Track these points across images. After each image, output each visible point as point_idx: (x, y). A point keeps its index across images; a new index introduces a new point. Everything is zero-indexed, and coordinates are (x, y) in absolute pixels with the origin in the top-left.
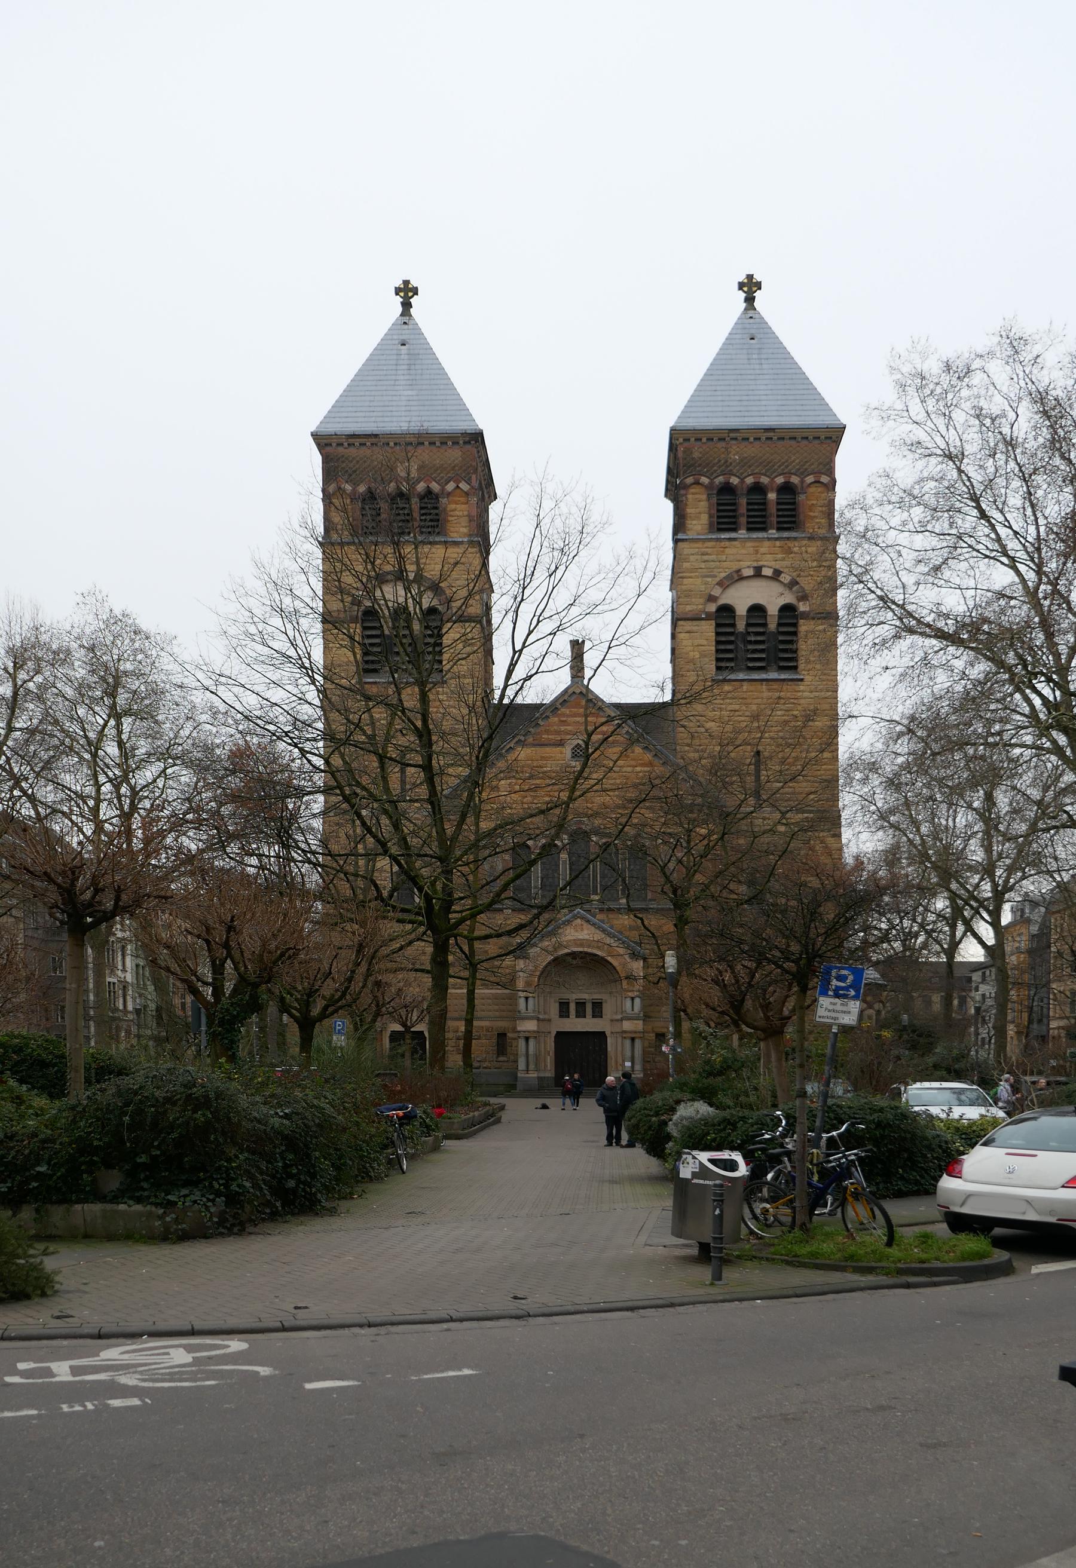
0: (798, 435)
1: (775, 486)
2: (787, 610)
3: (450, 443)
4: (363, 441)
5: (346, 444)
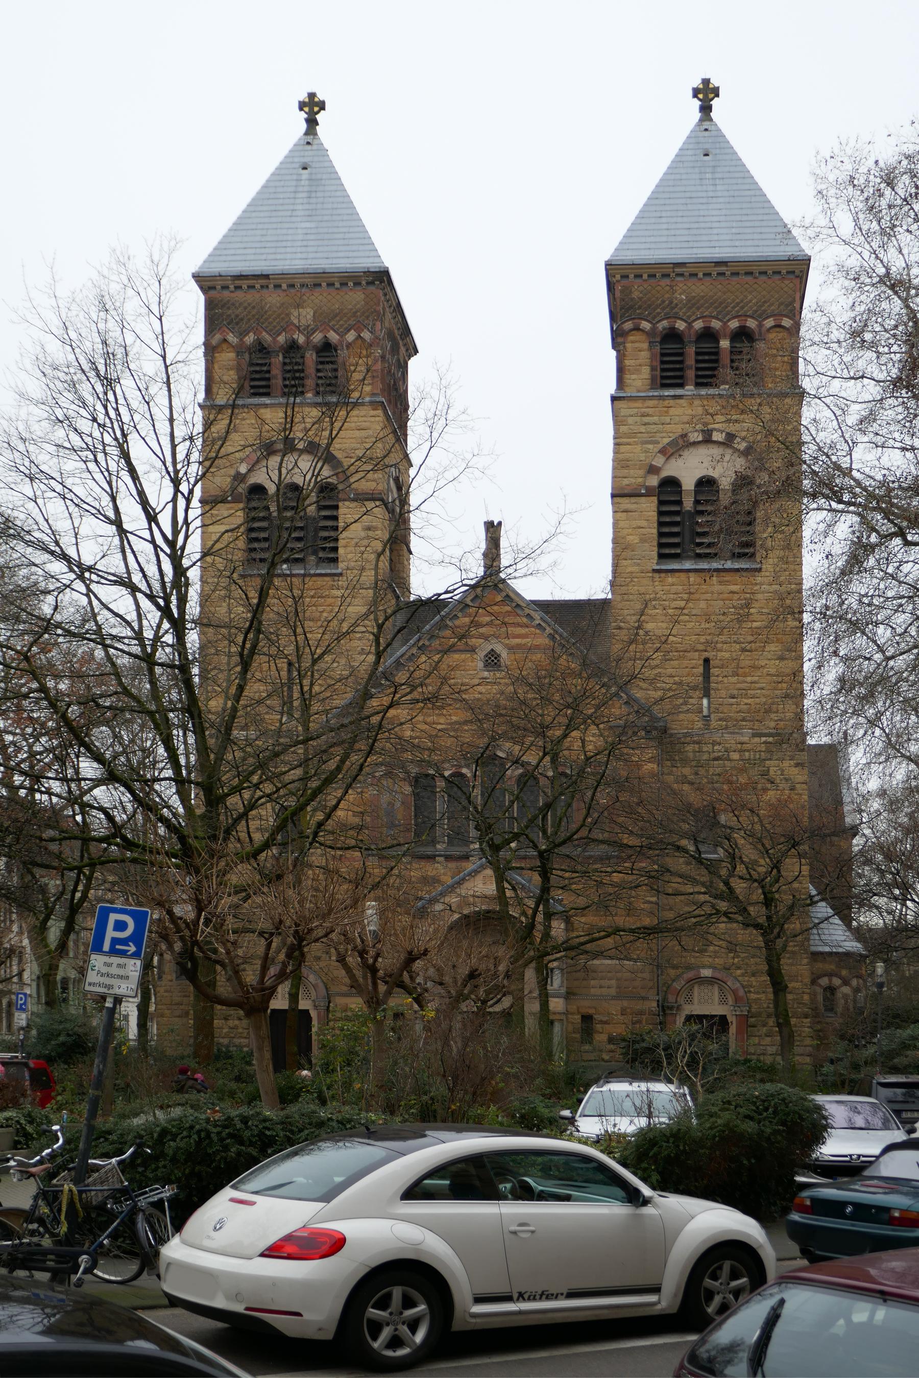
0: (755, 269)
3: (351, 284)
4: (251, 282)
5: (232, 287)
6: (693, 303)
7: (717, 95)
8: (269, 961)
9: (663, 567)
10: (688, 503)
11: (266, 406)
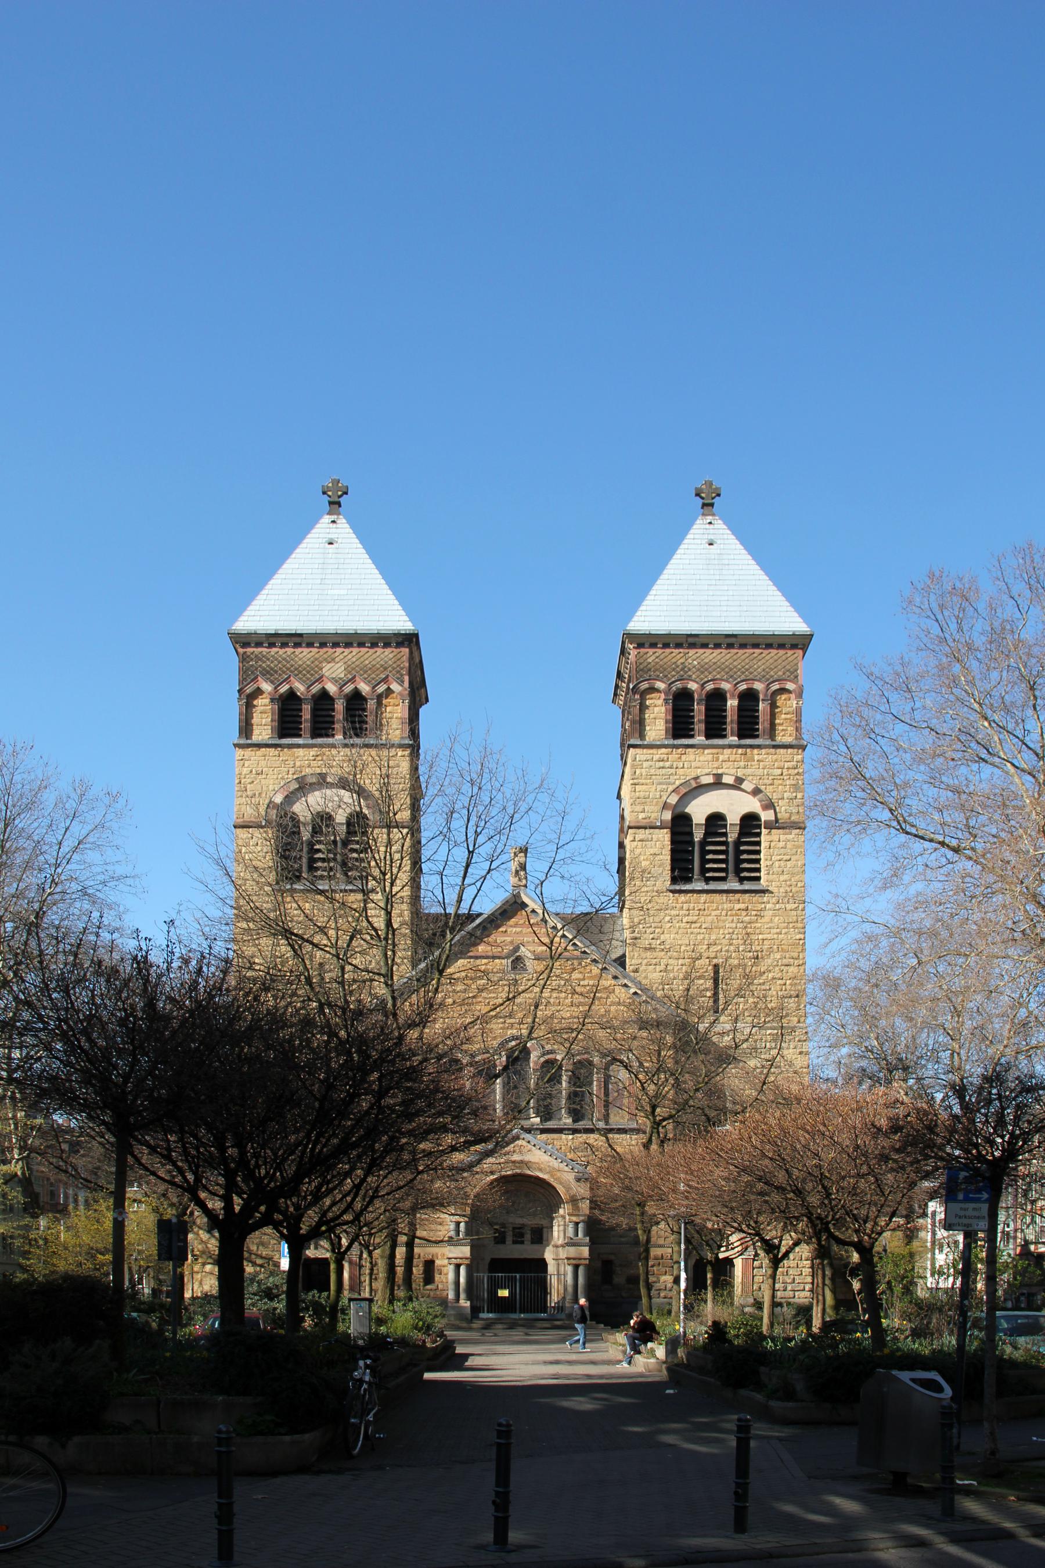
1: (737, 692)
2: (750, 821)
4: (285, 640)
6: (703, 669)
7: (719, 495)
8: (8, 1178)
9: (677, 887)
10: (698, 835)
11: (299, 746)
